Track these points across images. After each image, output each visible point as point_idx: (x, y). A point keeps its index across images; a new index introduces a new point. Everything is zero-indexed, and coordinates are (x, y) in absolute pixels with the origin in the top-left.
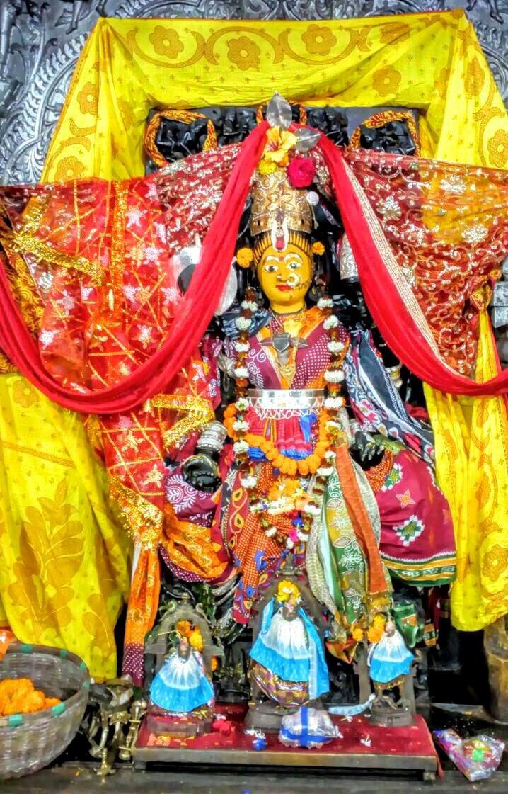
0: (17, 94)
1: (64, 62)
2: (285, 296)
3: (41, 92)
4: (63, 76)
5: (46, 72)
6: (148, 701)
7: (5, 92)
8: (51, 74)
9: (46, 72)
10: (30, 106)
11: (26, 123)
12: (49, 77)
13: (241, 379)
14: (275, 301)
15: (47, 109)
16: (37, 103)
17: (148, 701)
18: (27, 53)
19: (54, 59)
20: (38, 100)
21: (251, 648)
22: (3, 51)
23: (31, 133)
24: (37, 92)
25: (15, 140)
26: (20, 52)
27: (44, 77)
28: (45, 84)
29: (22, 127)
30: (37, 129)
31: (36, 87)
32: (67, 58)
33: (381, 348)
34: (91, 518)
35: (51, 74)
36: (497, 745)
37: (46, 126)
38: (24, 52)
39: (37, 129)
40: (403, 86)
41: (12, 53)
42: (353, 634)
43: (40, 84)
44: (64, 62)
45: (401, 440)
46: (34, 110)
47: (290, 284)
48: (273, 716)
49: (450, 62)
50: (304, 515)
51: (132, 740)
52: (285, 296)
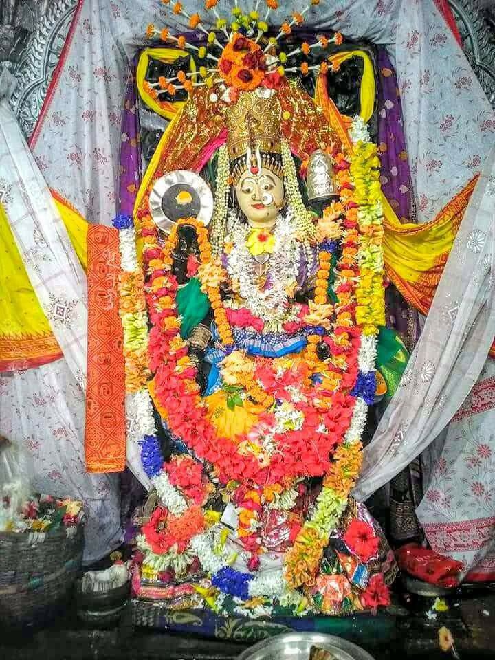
0: (27, 41)
1: (64, 10)
3: (44, 37)
4: (63, 23)
8: (53, 22)
10: (36, 50)
12: (51, 24)
13: (168, 194)
14: (251, 218)
15: (50, 52)
16: (42, 47)
20: (42, 45)
21: (439, 641)
23: (38, 74)
24: (41, 37)
27: (48, 25)
28: (48, 30)
30: (41, 70)
31: (41, 34)
33: (333, 272)
35: (53, 22)
36: (46, 518)
37: (51, 67)
39: (41, 70)
40: (427, 500)
42: (29, 331)
44: (64, 10)
45: (390, 425)
46: (40, 53)
50: (438, 589)
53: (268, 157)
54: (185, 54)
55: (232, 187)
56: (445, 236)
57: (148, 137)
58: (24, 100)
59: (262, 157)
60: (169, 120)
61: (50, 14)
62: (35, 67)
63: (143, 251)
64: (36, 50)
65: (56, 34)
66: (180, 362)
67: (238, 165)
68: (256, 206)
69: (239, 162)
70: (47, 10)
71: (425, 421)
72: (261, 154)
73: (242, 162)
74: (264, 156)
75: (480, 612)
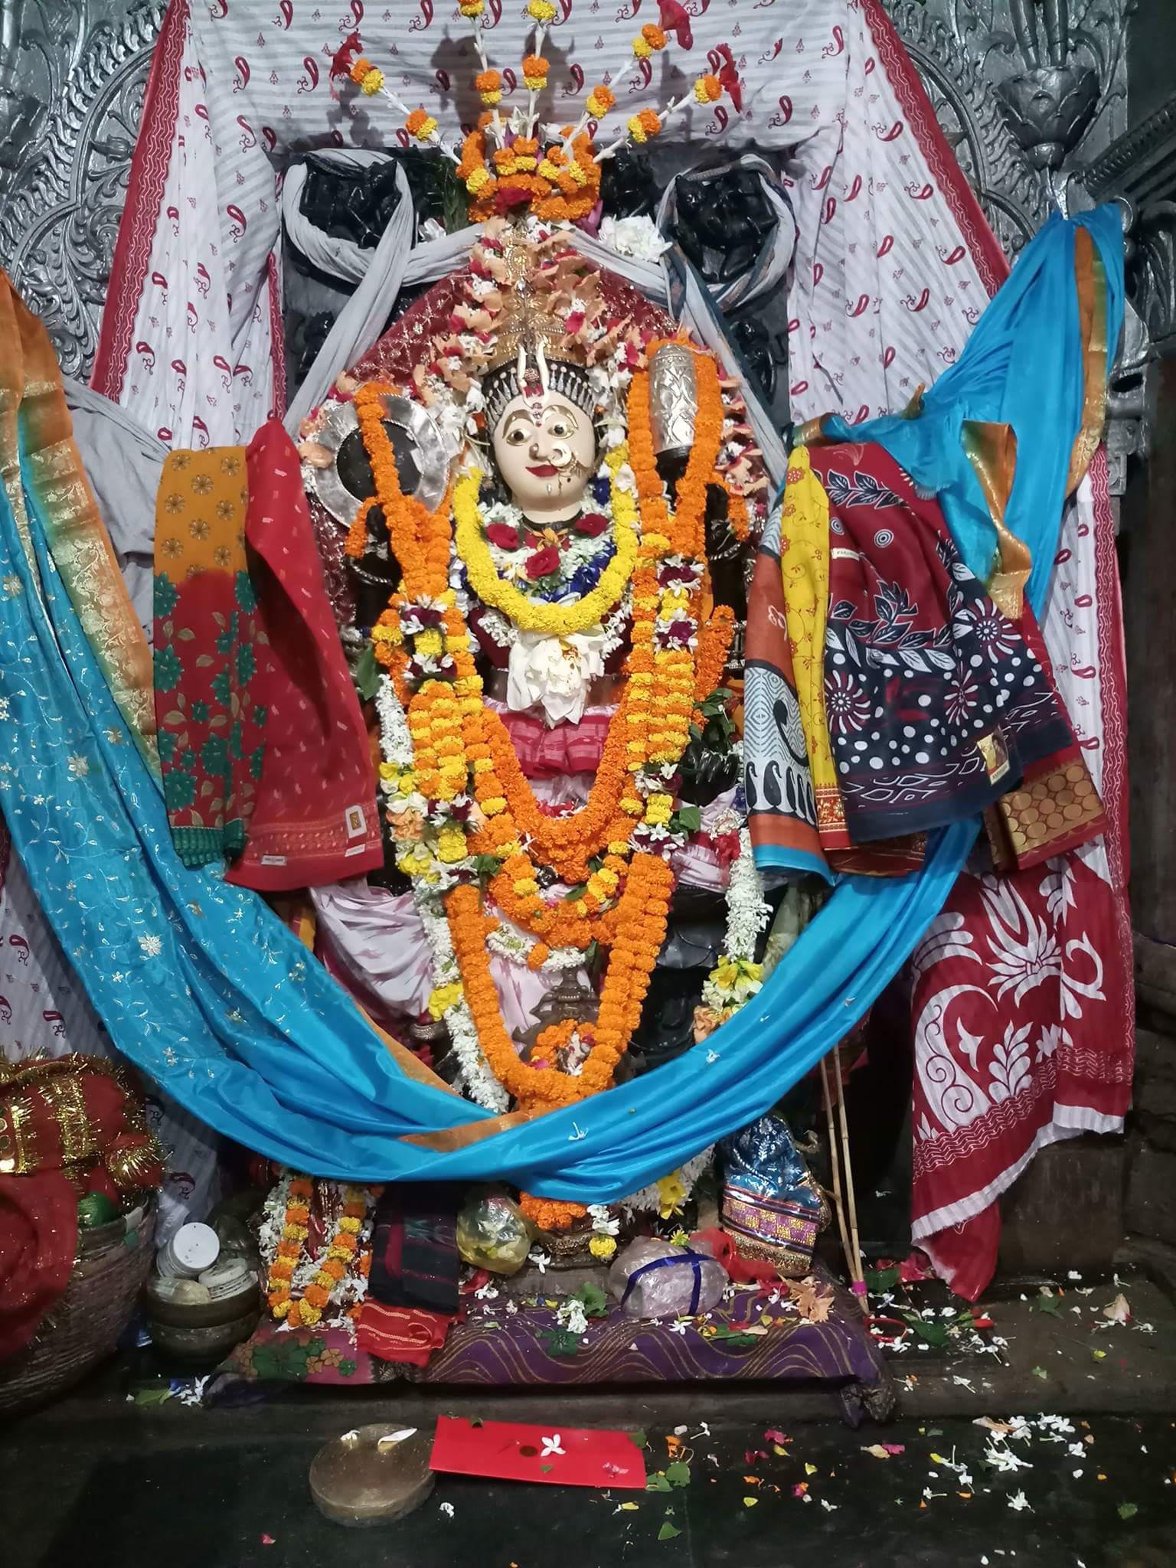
1: (122, 59)
2: (549, 486)
5: (89, 78)
6: (1012, 783)
7: (12, 118)
9: (89, 78)
11: (54, 174)
17: (1012, 783)
18: (54, 50)
19: (104, 52)
22: (7, 41)
23: (65, 194)
25: (33, 207)
26: (40, 46)
28: (86, 99)
29: (47, 181)
32: (129, 51)
34: (55, 617)
35: (99, 82)
38: (48, 48)
41: (27, 48)
43: (77, 101)
44: (122, 59)
47: (557, 463)
48: (672, 1268)
49: (842, 139)
51: (957, 325)
52: (549, 486)
53: (564, 369)
54: (384, 158)
55: (286, 393)
56: (1065, 546)
57: (301, 329)
58: (33, 248)
59: (550, 370)
60: (348, 288)
61: (91, 65)
62: (58, 178)
63: (115, 618)
64: (60, 143)
65: (104, 110)
66: (523, 881)
67: (495, 390)
68: (539, 472)
69: (503, 375)
70: (85, 55)
71: (860, 929)
72: (549, 362)
73: (509, 374)
74: (554, 367)
75: (1091, 1355)
